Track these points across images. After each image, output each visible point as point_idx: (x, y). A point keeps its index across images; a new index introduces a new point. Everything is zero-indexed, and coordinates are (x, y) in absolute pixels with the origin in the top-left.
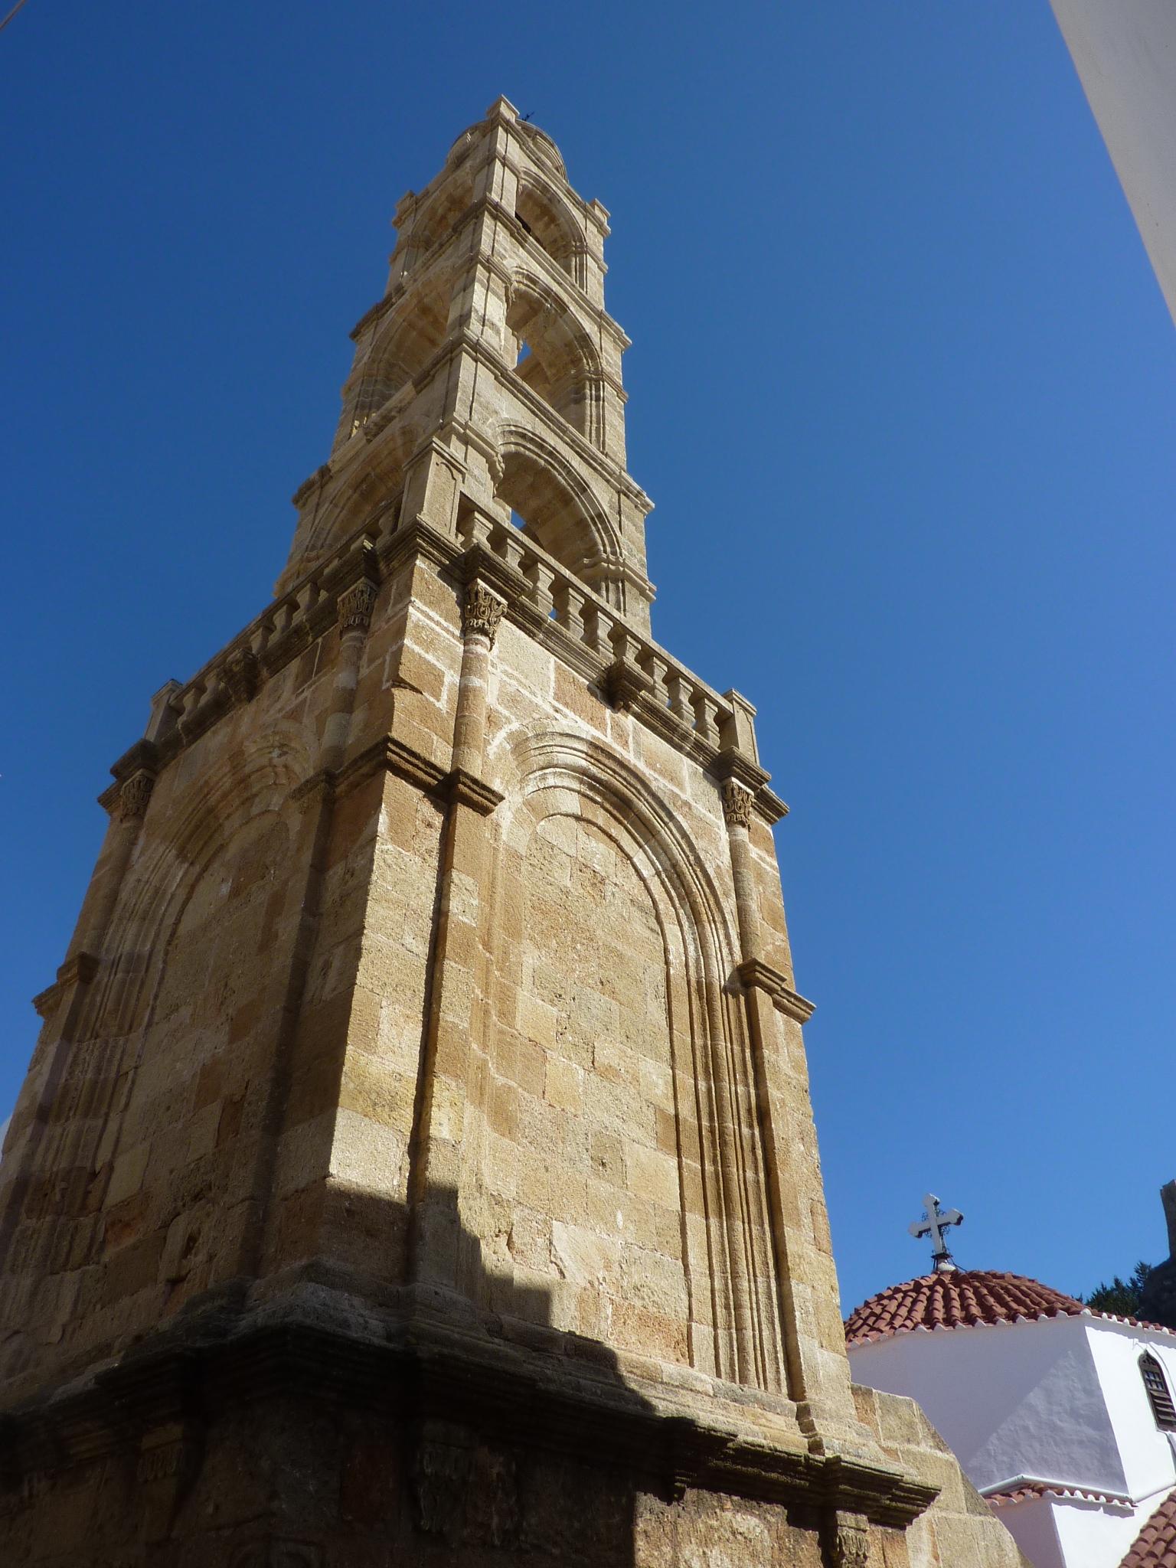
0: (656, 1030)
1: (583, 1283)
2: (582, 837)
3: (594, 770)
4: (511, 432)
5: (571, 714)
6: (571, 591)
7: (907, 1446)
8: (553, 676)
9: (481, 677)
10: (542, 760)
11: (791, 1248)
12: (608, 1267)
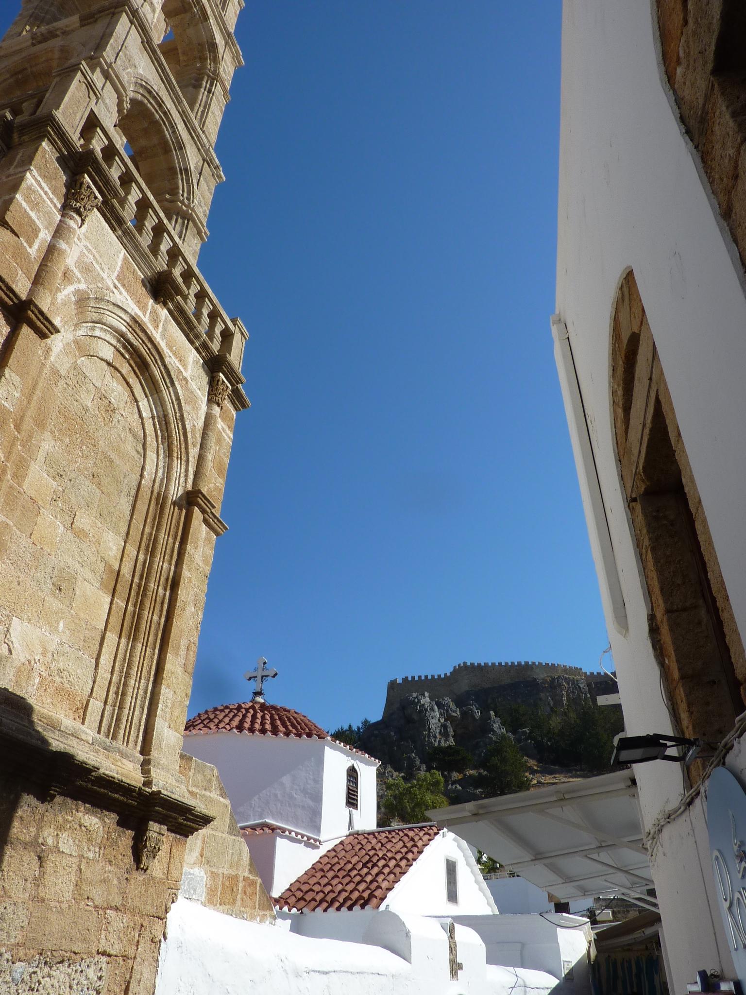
0: (122, 516)
1: (23, 660)
2: (108, 377)
3: (130, 336)
4: (141, 85)
5: (125, 293)
6: (150, 210)
7: (204, 792)
8: (120, 263)
9: (67, 243)
10: (95, 317)
11: (168, 666)
12: (44, 654)
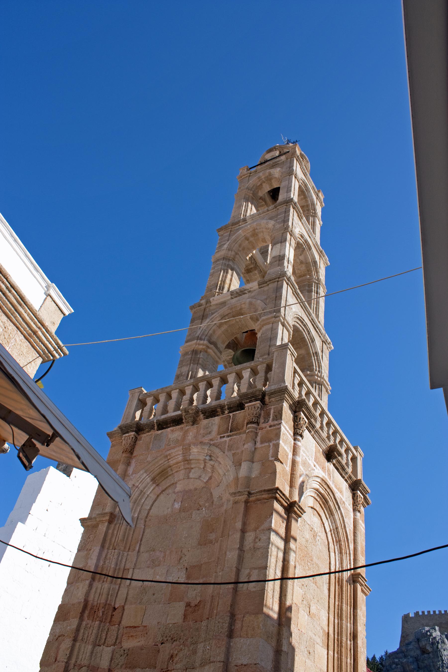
3: (321, 490)
8: (314, 450)
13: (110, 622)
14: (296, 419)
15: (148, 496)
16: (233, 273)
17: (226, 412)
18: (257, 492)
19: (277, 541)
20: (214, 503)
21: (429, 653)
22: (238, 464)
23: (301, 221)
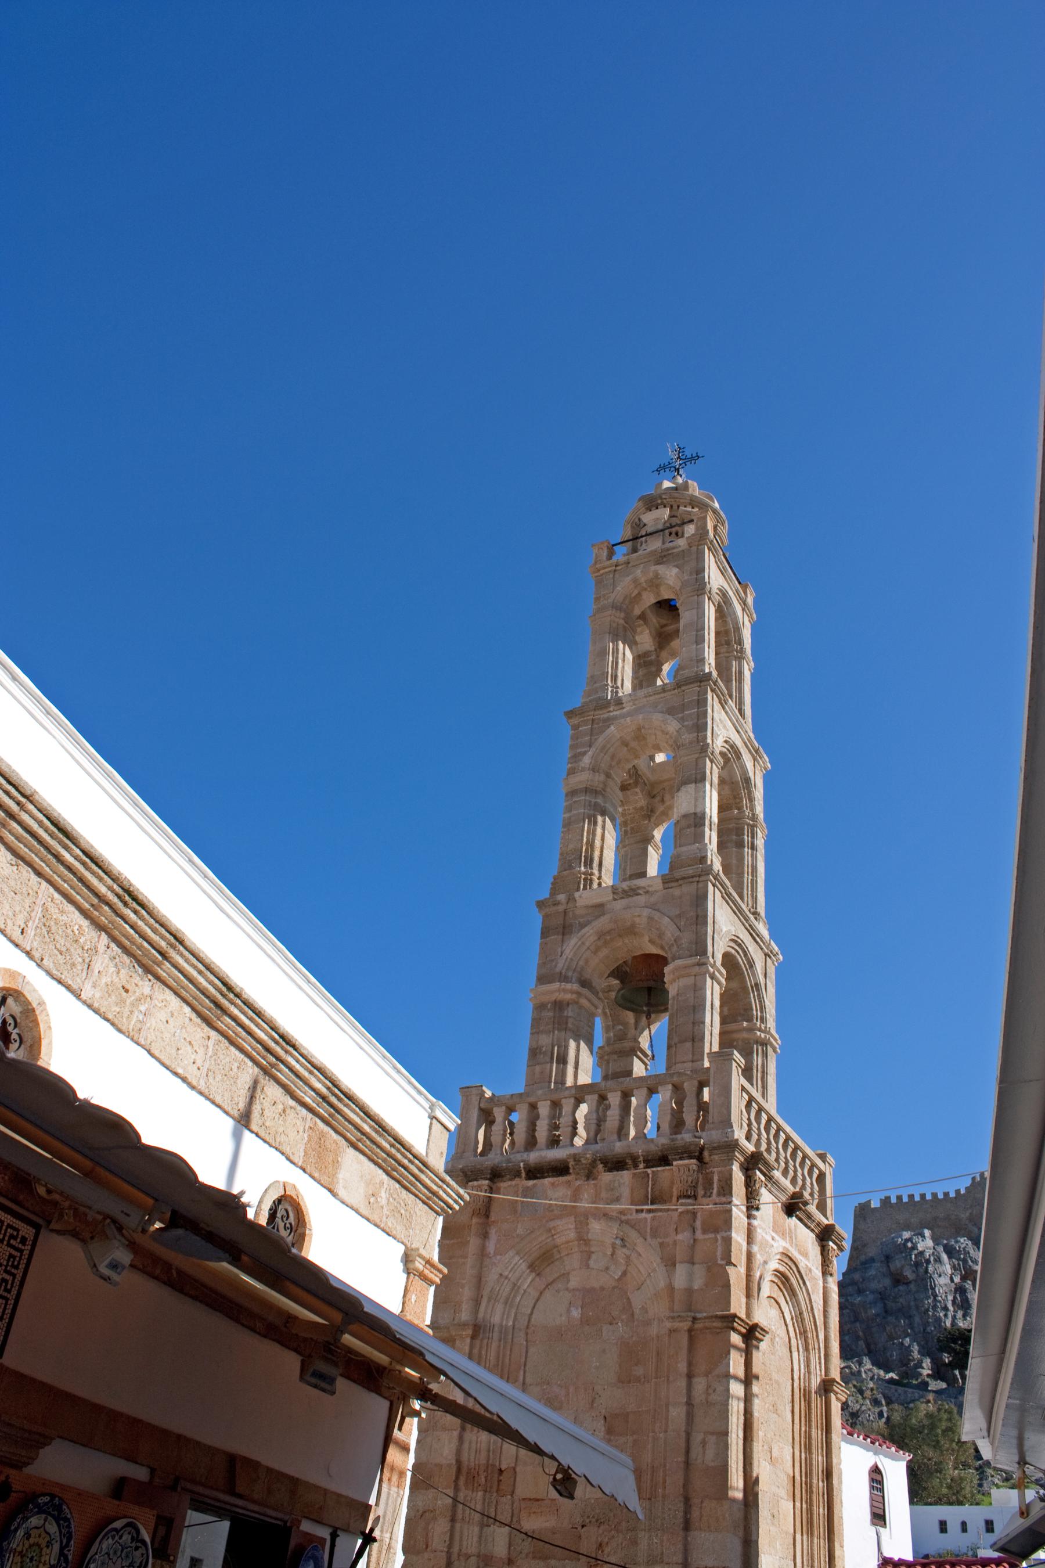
13: (497, 1491)
14: (749, 1182)
15: (525, 1291)
16: (604, 822)
17: (642, 1166)
18: (705, 1318)
19: (737, 1389)
20: (636, 1317)
21: (908, 1283)
22: (670, 1263)
23: (724, 708)
